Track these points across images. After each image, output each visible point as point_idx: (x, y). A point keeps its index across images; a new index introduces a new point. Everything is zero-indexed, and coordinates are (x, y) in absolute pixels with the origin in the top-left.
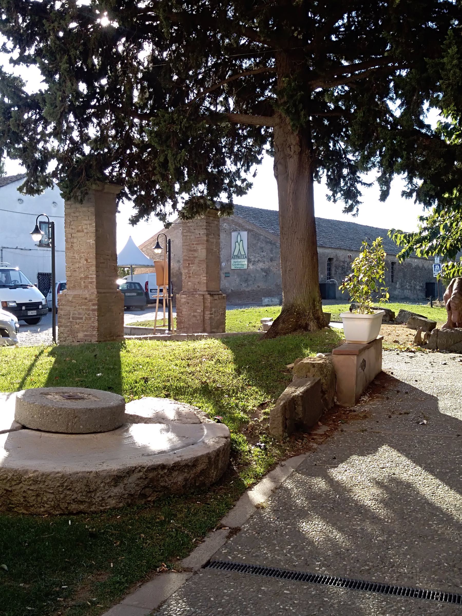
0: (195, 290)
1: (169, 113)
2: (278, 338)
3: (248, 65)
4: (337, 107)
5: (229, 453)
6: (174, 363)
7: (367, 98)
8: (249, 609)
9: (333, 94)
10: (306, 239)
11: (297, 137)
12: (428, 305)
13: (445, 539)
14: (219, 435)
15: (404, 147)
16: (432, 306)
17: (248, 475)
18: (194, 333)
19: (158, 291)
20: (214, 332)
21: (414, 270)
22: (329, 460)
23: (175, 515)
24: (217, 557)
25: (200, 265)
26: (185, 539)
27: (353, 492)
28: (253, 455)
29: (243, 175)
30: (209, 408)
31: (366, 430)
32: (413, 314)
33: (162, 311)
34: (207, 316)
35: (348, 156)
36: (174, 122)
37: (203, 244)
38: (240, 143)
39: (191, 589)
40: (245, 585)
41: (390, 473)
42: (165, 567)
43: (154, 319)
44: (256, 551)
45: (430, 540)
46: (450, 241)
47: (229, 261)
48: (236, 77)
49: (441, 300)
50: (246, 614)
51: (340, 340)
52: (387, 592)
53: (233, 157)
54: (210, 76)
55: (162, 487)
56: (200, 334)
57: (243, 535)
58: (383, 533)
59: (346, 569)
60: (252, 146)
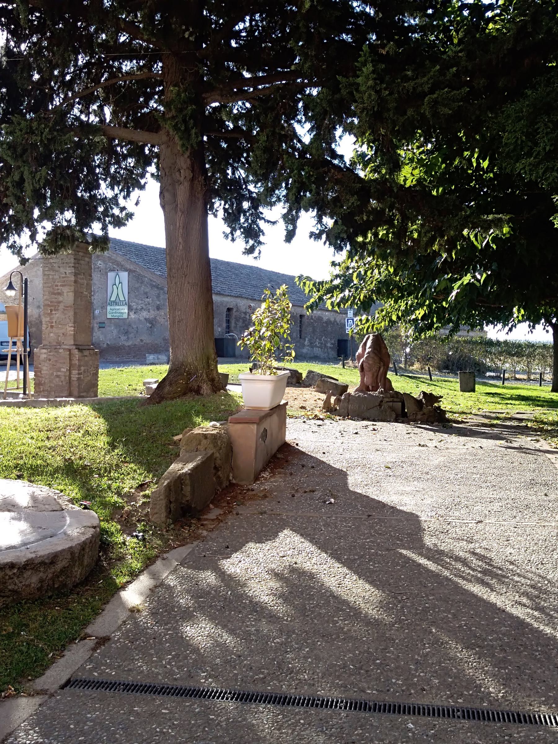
0: (59, 344)
1: (26, 120)
2: (163, 403)
3: (128, 68)
4: (236, 127)
5: (98, 546)
6: (29, 436)
7: (271, 118)
8: (117, 736)
9: (231, 110)
10: (199, 284)
11: (188, 160)
12: (340, 365)
13: (352, 637)
14: (85, 524)
15: (313, 179)
16: (344, 367)
17: (121, 572)
18: (56, 397)
19: (11, 344)
20: (83, 397)
21: (325, 325)
22: (220, 550)
23: (27, 626)
24: (80, 674)
25: (65, 312)
26: (39, 655)
27: (248, 587)
28: (128, 547)
29: (122, 202)
30: (74, 492)
31: (265, 513)
32: (322, 376)
33: (16, 370)
34: (75, 377)
35: (249, 187)
36: (32, 132)
37: (71, 286)
38: (118, 163)
39: (45, 716)
40: (114, 707)
41: (291, 562)
42: (12, 690)
43: (4, 380)
44: (129, 664)
45: (335, 639)
46: (365, 291)
47: (104, 307)
48: (114, 81)
49: (353, 360)
50: (114, 742)
51: (238, 405)
52: (283, 704)
53: (109, 179)
54: (80, 78)
55: (10, 591)
56: (64, 399)
57: (113, 645)
58: (282, 634)
59: (236, 680)
60: (133, 167)
